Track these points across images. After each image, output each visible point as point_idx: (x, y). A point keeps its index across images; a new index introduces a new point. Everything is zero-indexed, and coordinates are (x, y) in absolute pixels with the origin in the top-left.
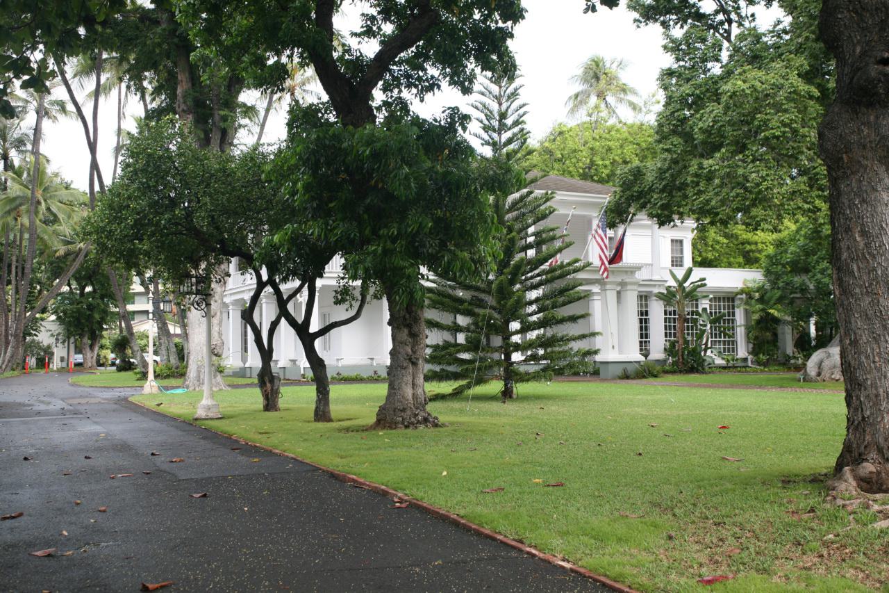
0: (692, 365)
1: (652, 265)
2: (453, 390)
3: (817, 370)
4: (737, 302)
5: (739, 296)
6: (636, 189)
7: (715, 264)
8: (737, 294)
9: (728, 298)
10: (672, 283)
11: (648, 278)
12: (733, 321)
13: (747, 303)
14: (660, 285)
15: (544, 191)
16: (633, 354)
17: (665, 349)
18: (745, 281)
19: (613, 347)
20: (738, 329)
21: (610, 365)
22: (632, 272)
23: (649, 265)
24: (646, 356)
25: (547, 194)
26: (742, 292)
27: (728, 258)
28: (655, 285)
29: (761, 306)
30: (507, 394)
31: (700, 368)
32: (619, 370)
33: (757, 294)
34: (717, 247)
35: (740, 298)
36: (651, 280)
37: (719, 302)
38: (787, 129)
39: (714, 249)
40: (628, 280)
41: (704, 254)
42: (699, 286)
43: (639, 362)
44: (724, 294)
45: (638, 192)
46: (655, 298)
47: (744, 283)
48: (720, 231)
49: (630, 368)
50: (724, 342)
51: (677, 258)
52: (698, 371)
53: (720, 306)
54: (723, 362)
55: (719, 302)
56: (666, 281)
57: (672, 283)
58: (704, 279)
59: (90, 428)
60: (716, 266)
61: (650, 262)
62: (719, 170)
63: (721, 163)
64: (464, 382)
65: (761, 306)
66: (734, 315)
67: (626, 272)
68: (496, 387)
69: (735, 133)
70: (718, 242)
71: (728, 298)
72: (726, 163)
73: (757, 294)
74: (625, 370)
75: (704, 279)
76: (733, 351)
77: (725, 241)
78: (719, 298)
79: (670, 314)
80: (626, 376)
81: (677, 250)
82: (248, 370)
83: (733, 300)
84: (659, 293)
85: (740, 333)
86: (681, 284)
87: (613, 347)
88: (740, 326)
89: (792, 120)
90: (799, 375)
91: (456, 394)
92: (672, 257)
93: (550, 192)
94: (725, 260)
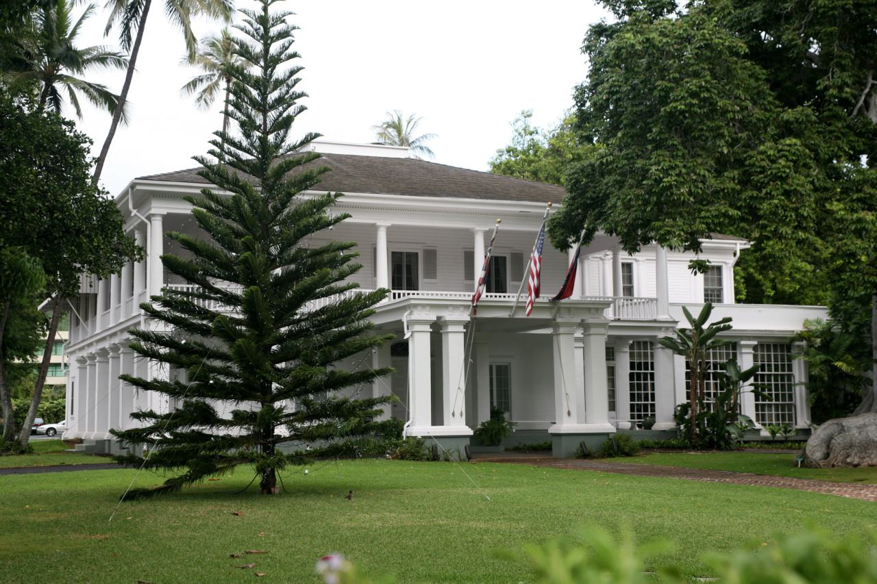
0: (711, 439)
1: (657, 300)
2: (167, 482)
3: (824, 450)
4: (794, 351)
5: (797, 343)
6: (588, 195)
7: (797, 299)
8: (793, 340)
9: (776, 347)
10: (686, 324)
11: (650, 318)
12: (790, 377)
13: (807, 354)
14: (667, 328)
15: (326, 193)
16: (602, 423)
17: (675, 416)
18: (806, 322)
19: (569, 414)
20: (797, 388)
21: (563, 437)
22: (597, 309)
23: (652, 300)
24: (648, 426)
25: (329, 195)
26: (800, 337)
27: (815, 291)
28: (660, 328)
29: (823, 357)
30: (268, 487)
31: (722, 443)
32: (574, 446)
33: (818, 340)
34: (798, 276)
35: (798, 346)
36: (655, 321)
37: (769, 350)
38: (695, 101)
39: (793, 279)
40: (590, 321)
41: (779, 286)
42: (719, 329)
43: (607, 434)
44: (773, 341)
45: (592, 198)
46: (660, 345)
47: (805, 325)
48: (807, 254)
49: (591, 445)
50: (777, 406)
51: (712, 290)
52: (719, 448)
53: (769, 356)
54: (765, 433)
55: (769, 350)
56: (677, 322)
57: (686, 324)
58: (730, 320)
59: (603, 466)
60: (798, 303)
61: (654, 296)
62: (611, 162)
63: (616, 153)
64: (185, 470)
65: (823, 357)
66: (790, 368)
67: (589, 309)
68: (246, 474)
69: (635, 109)
70: (798, 270)
71: (782, 346)
72: (624, 152)
73: (818, 340)
74: (582, 445)
75: (730, 320)
76: (790, 419)
77: (809, 267)
78: (768, 346)
79: (639, 368)
80: (585, 454)
81: (713, 280)
82: (107, 443)
83: (789, 348)
84: (666, 338)
85: (800, 394)
86: (697, 324)
87: (569, 414)
88: (801, 383)
89: (701, 87)
90: (794, 456)
91: (170, 490)
92: (706, 290)
93: (333, 193)
94: (811, 293)
